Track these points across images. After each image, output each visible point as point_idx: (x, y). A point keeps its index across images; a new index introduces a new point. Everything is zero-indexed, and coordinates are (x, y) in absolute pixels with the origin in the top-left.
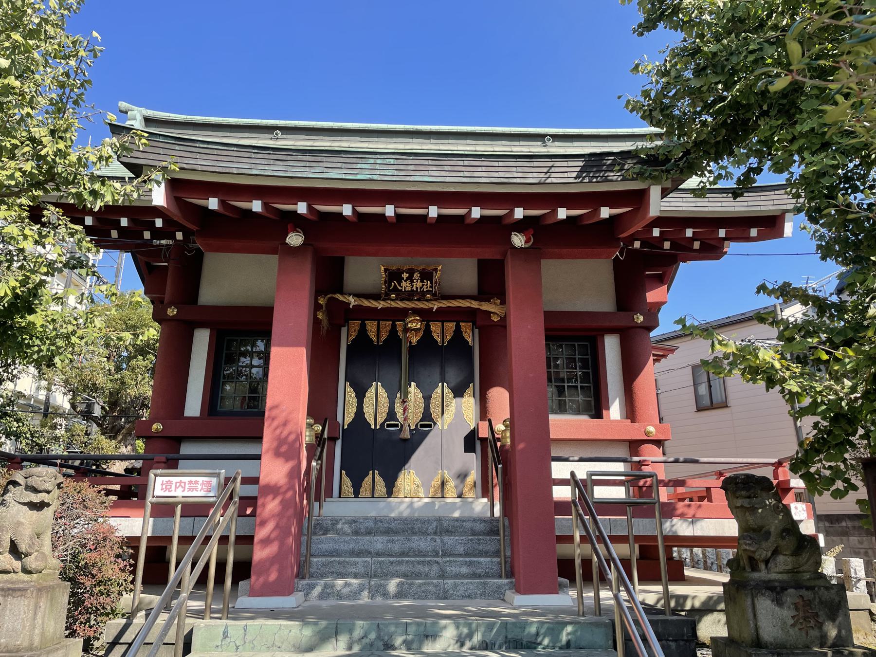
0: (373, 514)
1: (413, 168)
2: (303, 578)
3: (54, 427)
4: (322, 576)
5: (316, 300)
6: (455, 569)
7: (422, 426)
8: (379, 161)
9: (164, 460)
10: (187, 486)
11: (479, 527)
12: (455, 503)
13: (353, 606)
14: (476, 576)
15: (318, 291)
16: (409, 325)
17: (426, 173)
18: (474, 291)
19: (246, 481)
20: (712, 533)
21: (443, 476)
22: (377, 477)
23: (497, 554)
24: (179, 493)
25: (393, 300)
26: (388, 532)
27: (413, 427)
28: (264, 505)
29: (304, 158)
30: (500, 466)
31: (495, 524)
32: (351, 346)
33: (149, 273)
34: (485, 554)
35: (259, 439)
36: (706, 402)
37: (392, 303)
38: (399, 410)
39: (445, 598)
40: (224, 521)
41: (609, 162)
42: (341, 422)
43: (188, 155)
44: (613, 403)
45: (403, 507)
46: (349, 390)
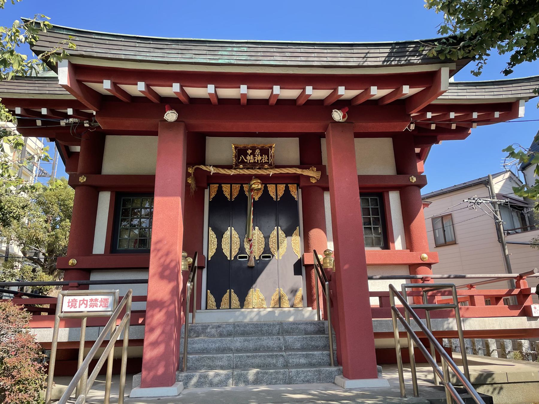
0: (231, 320)
1: (262, 54)
2: (182, 371)
3: (12, 268)
4: (196, 369)
5: (187, 170)
6: (296, 361)
7: (264, 257)
8: (235, 49)
9: (76, 285)
10: (89, 303)
11: (310, 328)
12: (289, 311)
13: (222, 392)
14: (311, 365)
15: (189, 164)
16: (253, 186)
17: (272, 58)
18: (298, 163)
19: (135, 299)
20: (478, 328)
21: (279, 292)
22: (233, 294)
23: (326, 347)
24: (82, 308)
25: (241, 169)
27: (257, 258)
28: (152, 316)
29: (177, 47)
30: (327, 283)
31: (322, 325)
32: (214, 201)
33: (68, 157)
34: (316, 348)
35: (146, 269)
36: (442, 241)
37: (241, 171)
38: (247, 246)
39: (290, 383)
40: (119, 329)
41: (411, 49)
42: (206, 256)
43: (86, 44)
44: (397, 238)
45: (253, 315)
46: (212, 233)
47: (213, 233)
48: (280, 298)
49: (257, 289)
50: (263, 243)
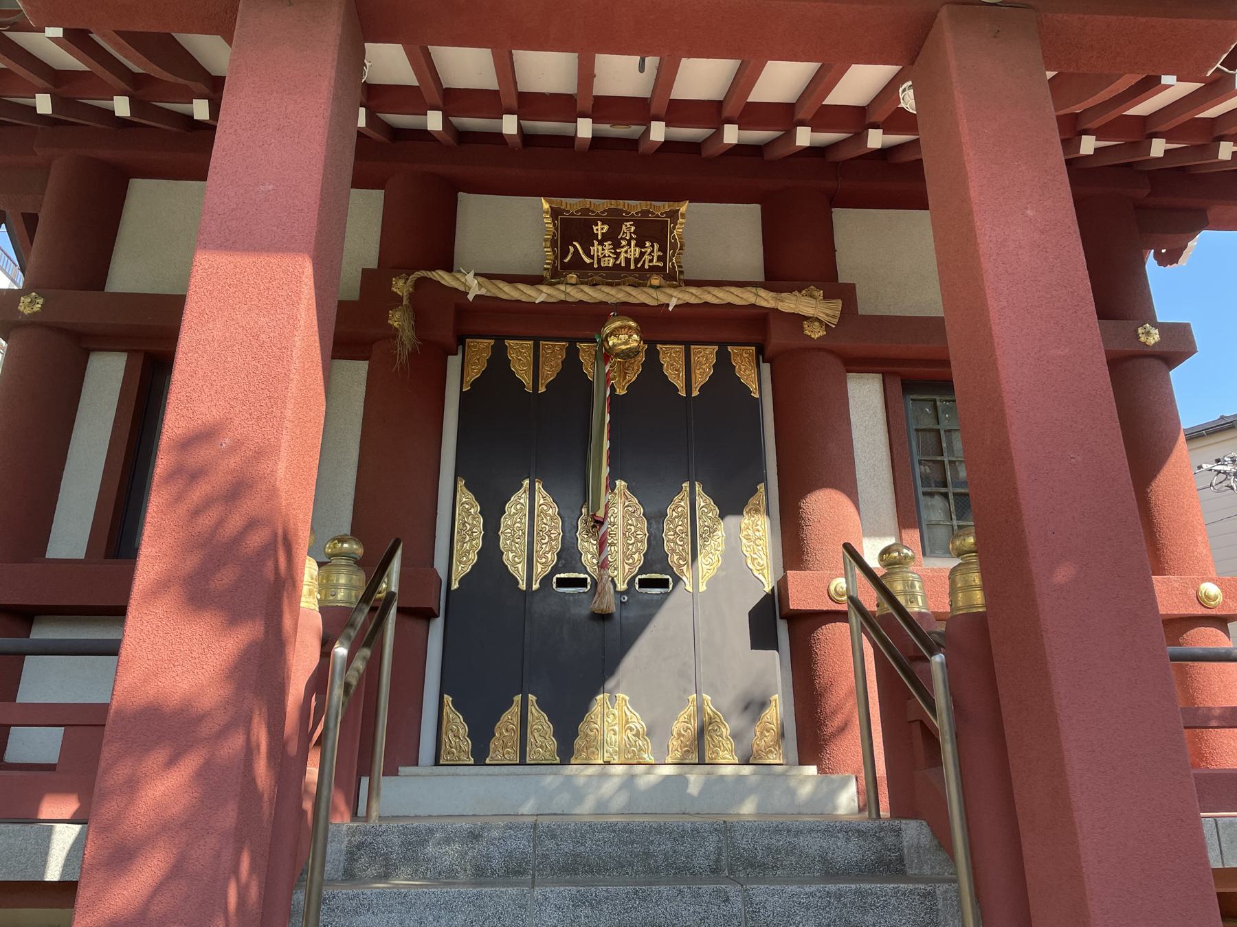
11: (846, 851)
12: (740, 778)
16: (612, 341)
21: (700, 709)
22: (534, 710)
28: (132, 786)
30: (938, 658)
31: (890, 839)
37: (569, 289)
38: (587, 547)
45: (608, 788)
46: (466, 497)
47: (471, 496)
48: (701, 733)
49: (620, 695)
50: (643, 534)
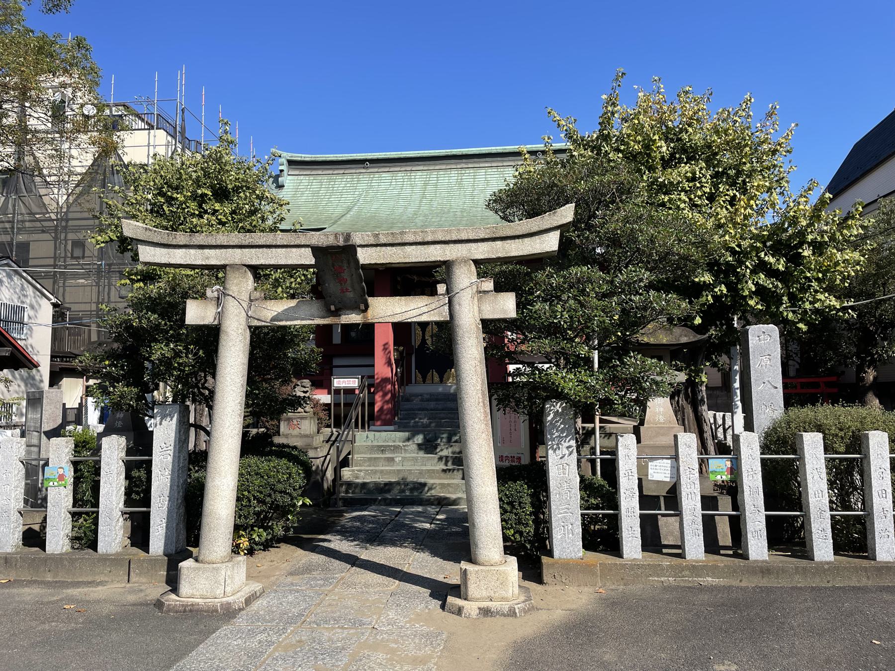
26: (437, 400)
